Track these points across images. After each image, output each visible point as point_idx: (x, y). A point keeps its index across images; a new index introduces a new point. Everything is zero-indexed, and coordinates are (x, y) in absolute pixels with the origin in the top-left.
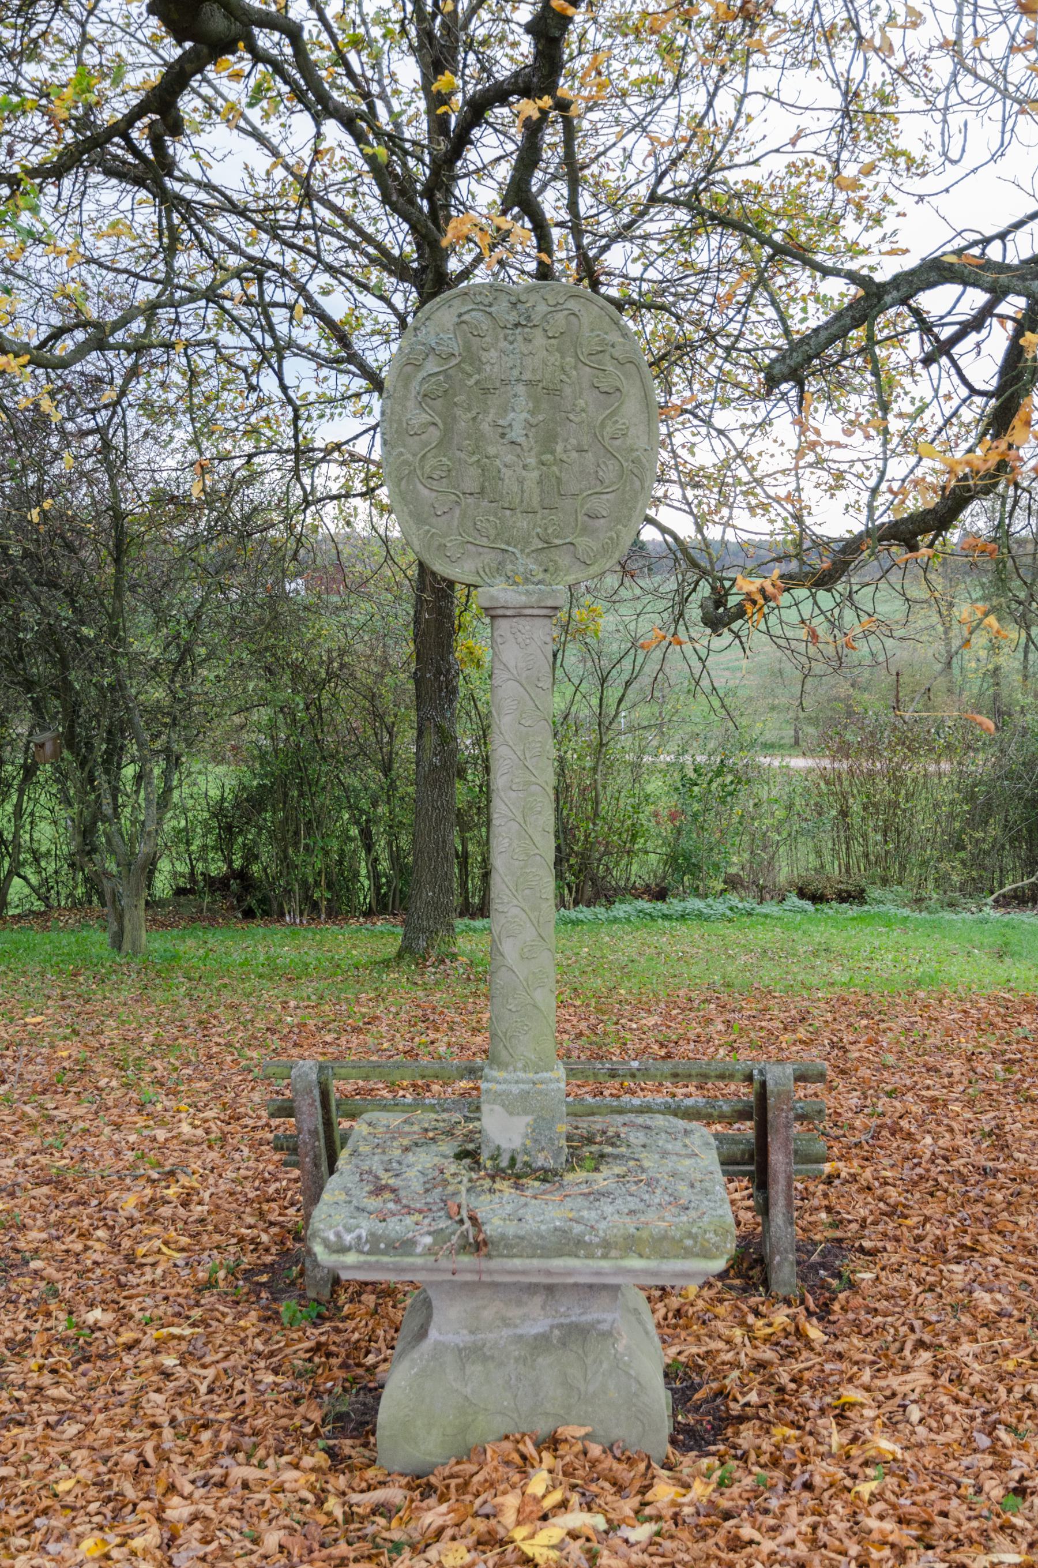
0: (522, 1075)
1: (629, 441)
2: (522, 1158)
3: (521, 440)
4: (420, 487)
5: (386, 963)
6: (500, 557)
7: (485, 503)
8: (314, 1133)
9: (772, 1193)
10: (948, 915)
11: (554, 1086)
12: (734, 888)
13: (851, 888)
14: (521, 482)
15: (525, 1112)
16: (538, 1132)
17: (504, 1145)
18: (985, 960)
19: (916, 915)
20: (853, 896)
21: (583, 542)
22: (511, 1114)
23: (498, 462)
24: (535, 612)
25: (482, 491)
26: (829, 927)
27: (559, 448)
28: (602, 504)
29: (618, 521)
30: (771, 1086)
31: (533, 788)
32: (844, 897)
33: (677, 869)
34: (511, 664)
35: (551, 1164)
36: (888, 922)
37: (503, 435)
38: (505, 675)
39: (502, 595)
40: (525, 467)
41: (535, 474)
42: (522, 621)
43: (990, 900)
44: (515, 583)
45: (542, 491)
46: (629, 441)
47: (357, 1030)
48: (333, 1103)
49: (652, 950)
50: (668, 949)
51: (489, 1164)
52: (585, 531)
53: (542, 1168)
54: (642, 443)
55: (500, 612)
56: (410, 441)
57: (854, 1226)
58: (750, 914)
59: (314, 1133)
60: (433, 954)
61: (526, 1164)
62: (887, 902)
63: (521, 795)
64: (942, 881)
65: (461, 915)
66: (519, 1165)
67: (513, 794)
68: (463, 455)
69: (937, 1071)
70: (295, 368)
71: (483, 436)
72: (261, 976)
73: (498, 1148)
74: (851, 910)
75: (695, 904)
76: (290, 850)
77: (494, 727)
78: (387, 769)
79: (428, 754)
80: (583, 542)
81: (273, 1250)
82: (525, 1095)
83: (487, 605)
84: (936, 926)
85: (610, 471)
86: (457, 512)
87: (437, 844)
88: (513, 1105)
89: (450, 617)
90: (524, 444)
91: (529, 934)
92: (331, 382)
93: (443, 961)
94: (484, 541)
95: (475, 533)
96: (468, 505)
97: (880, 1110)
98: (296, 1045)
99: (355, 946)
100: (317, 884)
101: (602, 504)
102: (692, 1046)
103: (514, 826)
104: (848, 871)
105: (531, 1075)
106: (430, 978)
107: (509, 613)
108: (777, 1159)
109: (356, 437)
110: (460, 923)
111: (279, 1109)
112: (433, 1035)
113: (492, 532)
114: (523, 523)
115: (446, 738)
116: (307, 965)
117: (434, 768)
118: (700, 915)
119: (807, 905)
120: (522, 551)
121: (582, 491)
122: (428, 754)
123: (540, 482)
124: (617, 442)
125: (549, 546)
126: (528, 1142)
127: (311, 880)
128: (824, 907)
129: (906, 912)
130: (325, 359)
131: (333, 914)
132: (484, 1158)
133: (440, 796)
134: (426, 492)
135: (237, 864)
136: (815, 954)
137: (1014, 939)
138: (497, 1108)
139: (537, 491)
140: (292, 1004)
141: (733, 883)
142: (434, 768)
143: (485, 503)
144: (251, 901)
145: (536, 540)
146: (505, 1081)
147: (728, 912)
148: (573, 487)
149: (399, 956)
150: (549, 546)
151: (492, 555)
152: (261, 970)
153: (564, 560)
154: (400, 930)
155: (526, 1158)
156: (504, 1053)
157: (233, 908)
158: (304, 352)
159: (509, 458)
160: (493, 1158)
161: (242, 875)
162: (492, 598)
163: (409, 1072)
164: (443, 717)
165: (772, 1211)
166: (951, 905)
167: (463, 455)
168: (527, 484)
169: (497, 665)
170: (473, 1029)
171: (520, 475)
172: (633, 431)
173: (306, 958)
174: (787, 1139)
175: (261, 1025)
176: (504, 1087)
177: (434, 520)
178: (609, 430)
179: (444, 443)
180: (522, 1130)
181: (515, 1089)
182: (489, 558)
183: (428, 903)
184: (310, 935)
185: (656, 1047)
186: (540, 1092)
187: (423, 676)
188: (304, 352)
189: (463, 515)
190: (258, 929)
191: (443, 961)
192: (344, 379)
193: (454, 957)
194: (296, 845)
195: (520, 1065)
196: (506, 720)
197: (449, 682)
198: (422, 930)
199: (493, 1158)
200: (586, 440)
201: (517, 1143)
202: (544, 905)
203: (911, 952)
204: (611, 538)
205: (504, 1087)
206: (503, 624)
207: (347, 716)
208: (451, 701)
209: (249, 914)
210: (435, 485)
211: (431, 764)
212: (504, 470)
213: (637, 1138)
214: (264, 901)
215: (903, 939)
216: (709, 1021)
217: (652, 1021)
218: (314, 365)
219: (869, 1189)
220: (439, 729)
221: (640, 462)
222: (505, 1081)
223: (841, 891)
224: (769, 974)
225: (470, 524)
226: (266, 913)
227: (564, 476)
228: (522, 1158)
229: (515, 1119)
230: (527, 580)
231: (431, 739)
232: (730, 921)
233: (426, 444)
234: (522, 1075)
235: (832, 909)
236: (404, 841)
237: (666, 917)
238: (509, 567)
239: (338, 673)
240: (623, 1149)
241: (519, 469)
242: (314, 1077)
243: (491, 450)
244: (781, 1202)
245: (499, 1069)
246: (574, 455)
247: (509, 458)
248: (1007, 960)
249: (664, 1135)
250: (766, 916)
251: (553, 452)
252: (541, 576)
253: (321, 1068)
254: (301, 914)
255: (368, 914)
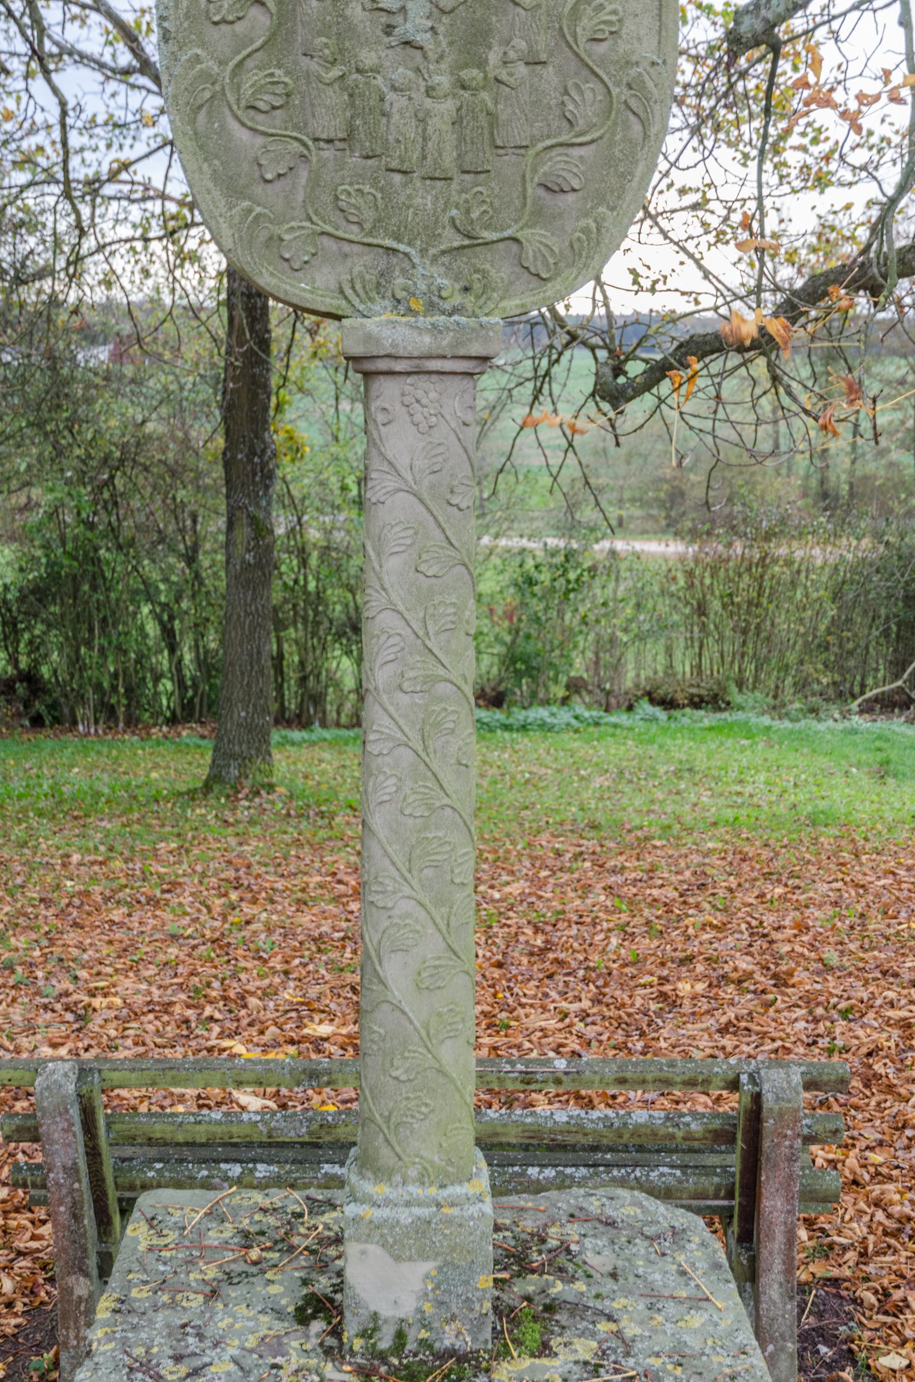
0: (416, 1190)
1: (622, 47)
2: (416, 1334)
3: (422, 38)
4: (234, 125)
5: (191, 795)
6: (382, 264)
7: (354, 160)
8: (72, 1171)
9: (764, 1253)
10: (809, 723)
11: (473, 1210)
12: (578, 692)
13: (704, 692)
14: (422, 120)
15: (423, 1256)
16: (441, 1291)
17: (386, 1311)
18: (866, 782)
19: (777, 724)
20: (711, 700)
21: (534, 237)
22: (398, 1258)
23: (379, 81)
24: (448, 365)
25: (349, 138)
26: (689, 740)
27: (493, 58)
28: (569, 165)
29: (600, 198)
30: (769, 1101)
31: (443, 688)
32: (697, 703)
33: (519, 674)
34: (402, 463)
35: (467, 1343)
36: (749, 732)
37: (389, 29)
38: (391, 483)
39: (386, 332)
40: (429, 92)
41: (448, 106)
42: (423, 382)
43: (855, 706)
44: (410, 311)
45: (461, 139)
46: (622, 47)
47: (154, 902)
48: (101, 1123)
49: (494, 770)
50: (512, 768)
51: (358, 1344)
52: (539, 216)
53: (451, 1353)
54: (647, 50)
55: (382, 365)
56: (213, 34)
57: (851, 1256)
58: (597, 724)
59: (72, 1171)
60: (247, 783)
61: (423, 1343)
62: (750, 711)
63: (417, 699)
64: (802, 686)
65: (277, 722)
66: (411, 1346)
67: (405, 699)
68: (313, 66)
69: (896, 975)
70: (75, 81)
71: (351, 28)
72: (41, 814)
73: (375, 1316)
74: (706, 718)
75: (539, 713)
76: (83, 650)
77: (370, 578)
78: (190, 559)
79: (240, 549)
80: (534, 237)
81: (19, 1307)
82: (422, 1227)
83: (358, 350)
84: (803, 738)
85: (587, 104)
86: (303, 175)
87: (251, 655)
88: (400, 1244)
89: (265, 387)
90: (429, 46)
91: (431, 947)
92: (121, 99)
93: (258, 793)
94: (354, 233)
95: (336, 217)
96: (323, 163)
97: (839, 1043)
98: (75, 925)
99: (156, 766)
100: (114, 688)
101: (569, 165)
102: (574, 931)
103: (406, 755)
104: (700, 672)
105: (433, 1191)
106: (243, 814)
107: (399, 366)
108: (774, 1204)
109: (147, 156)
110: (276, 736)
111: (19, 1130)
112: (248, 910)
113: (369, 215)
114: (424, 199)
115: (261, 530)
116: (97, 794)
117: (247, 567)
118: (544, 727)
119: (658, 712)
120: (423, 252)
121: (534, 140)
122: (240, 549)
123: (457, 122)
124: (601, 48)
125: (473, 242)
126: (428, 1307)
127: (106, 685)
128: (677, 713)
129: (766, 720)
130: (113, 70)
131: (132, 722)
132: (350, 1330)
133: (254, 599)
134: (243, 135)
135: (24, 662)
136: (678, 774)
137: (893, 755)
138: (373, 1249)
139: (451, 139)
140: (76, 858)
141: (575, 686)
142: (247, 567)
143: (354, 160)
144: (39, 706)
145: (449, 232)
146: (388, 1202)
147: (574, 722)
148: (518, 133)
149: (207, 788)
150: (473, 242)
151: (369, 257)
152: (41, 805)
153: (500, 270)
154: (209, 744)
155: (424, 1334)
156: (385, 1151)
157: (19, 715)
158: (83, 59)
159: (402, 74)
160: (364, 1334)
161: (30, 678)
162: (369, 338)
163: (218, 1076)
164: (258, 505)
165: (763, 1281)
166: (814, 710)
167: (313, 66)
168: (435, 123)
169: (376, 463)
170: (298, 901)
171: (420, 107)
172: (629, 27)
173: (98, 786)
174: (790, 1177)
175: (33, 894)
176: (385, 1213)
177: (259, 190)
178: (586, 25)
179: (277, 40)
180: (418, 1286)
181: (405, 1216)
182: (362, 263)
183: (240, 725)
184: (105, 750)
185: (529, 931)
186: (449, 1221)
187: (234, 457)
188: (83, 59)
189: (315, 182)
190: (46, 740)
191: (258, 793)
192: (135, 99)
193: (271, 788)
194: (89, 644)
195: (413, 1173)
196: (393, 564)
197: (264, 465)
198: (233, 756)
199: (364, 1334)
200: (544, 42)
201: (407, 1308)
202: (459, 895)
203: (783, 772)
204: (586, 231)
205: (385, 1213)
206: (388, 391)
207: (142, 506)
208: (267, 487)
209: (37, 722)
210: (261, 122)
211: (243, 561)
212: (391, 96)
213: (597, 1254)
214: (54, 706)
215: (772, 755)
216: (587, 889)
217: (515, 889)
218: (101, 78)
219: (855, 1182)
220: (253, 520)
221: (643, 87)
222: (388, 1202)
223: (692, 696)
224: (632, 807)
225: (327, 198)
226: (57, 720)
227: (503, 112)
228: (416, 1334)
229: (405, 1267)
230: (431, 307)
231: (243, 533)
232: (576, 731)
233: (241, 42)
234: (416, 1190)
235: (688, 716)
236: (212, 641)
237: (507, 728)
238: (400, 281)
239: (130, 455)
240: (580, 1286)
241: (418, 96)
242: (71, 1088)
243: (368, 58)
244: (778, 1266)
245: (378, 1180)
246: (522, 70)
247: (402, 74)
248: (890, 781)
249: (641, 1245)
250: (615, 726)
251: (481, 64)
252: (457, 300)
253: (83, 1072)
254: (96, 722)
255: (173, 721)
